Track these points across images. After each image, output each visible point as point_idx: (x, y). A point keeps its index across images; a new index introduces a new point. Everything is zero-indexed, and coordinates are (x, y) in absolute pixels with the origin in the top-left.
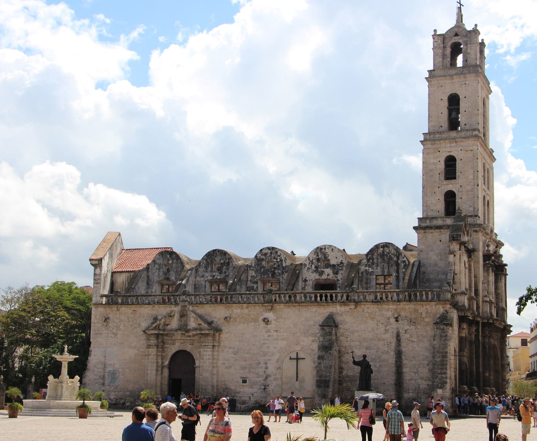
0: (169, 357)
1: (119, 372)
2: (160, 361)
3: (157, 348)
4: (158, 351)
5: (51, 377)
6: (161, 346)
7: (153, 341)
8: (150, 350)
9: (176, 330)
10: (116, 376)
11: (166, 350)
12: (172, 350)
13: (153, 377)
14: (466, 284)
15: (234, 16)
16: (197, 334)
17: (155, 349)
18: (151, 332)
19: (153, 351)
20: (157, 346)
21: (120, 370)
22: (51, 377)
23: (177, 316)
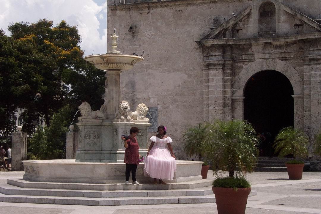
0: (243, 83)
2: (229, 90)
3: (224, 70)
4: (224, 74)
5: (84, 108)
6: (230, 68)
7: (216, 57)
8: (211, 72)
9: (256, 38)
11: (237, 71)
12: (248, 71)
13: (219, 117)
14: (239, 60)
15: (208, 170)
16: (294, 43)
17: (221, 71)
18: (210, 43)
19: (216, 77)
20: (224, 66)
21: (159, 107)
22: (84, 108)
23: (255, 15)
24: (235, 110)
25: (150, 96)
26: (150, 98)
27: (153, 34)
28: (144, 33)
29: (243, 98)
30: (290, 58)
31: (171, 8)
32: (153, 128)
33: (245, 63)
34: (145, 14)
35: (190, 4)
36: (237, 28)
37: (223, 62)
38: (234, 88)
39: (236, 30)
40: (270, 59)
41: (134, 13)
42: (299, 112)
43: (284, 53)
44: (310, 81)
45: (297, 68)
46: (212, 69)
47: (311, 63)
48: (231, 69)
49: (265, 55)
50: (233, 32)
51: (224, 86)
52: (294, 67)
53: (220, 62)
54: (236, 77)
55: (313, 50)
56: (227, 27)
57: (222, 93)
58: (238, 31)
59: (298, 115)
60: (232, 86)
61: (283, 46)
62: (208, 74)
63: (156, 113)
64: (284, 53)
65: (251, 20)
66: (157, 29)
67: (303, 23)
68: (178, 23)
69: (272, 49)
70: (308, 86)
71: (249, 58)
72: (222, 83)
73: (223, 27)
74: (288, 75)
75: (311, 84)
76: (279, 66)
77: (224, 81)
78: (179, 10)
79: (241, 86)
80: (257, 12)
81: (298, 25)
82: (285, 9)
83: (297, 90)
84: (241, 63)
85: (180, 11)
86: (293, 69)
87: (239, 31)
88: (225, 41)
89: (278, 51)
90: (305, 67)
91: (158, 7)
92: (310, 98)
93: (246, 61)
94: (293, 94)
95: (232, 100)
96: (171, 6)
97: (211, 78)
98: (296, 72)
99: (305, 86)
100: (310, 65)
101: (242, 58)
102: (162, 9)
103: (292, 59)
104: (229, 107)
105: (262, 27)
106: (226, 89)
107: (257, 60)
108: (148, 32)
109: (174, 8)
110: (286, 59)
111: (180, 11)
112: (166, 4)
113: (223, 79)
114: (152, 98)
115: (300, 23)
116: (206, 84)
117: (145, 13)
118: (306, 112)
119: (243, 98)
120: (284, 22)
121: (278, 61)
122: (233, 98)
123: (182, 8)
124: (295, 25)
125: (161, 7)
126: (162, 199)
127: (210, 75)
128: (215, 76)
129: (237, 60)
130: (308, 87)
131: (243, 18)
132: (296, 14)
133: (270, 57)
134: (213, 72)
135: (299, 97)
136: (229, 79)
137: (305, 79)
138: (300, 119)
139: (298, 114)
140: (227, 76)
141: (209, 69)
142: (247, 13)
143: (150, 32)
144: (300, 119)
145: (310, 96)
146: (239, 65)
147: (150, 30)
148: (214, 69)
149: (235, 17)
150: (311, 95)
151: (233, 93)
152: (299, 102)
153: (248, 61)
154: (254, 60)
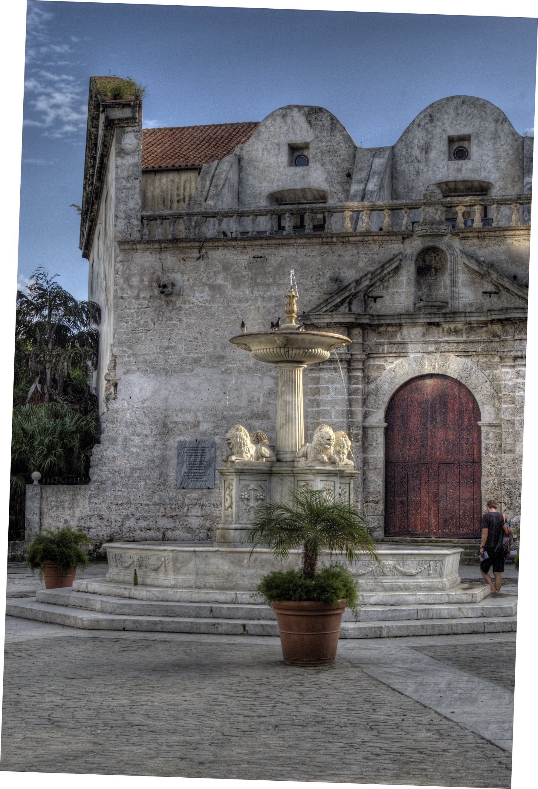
1: (213, 445)
2: (358, 409)
8: (326, 375)
10: (207, 458)
17: (342, 373)
21: (217, 439)
24: (368, 448)
25: (201, 419)
26: (199, 422)
27: (206, 300)
28: (189, 296)
29: (385, 425)
30: (474, 353)
31: (244, 251)
32: (204, 479)
33: (390, 360)
34: (192, 260)
35: (283, 245)
36: (375, 294)
37: (349, 356)
38: (367, 407)
39: (372, 297)
40: (436, 354)
41: (170, 259)
42: (491, 455)
43: (465, 342)
44: (514, 397)
45: (488, 371)
46: (326, 369)
47: (517, 363)
48: (363, 370)
49: (427, 345)
50: (365, 301)
51: (350, 403)
52: (483, 370)
53: (343, 356)
54: (372, 386)
55: (521, 340)
56: (357, 290)
57: (345, 416)
58: (375, 299)
59: (489, 460)
60: (364, 402)
61: (462, 330)
62: (319, 378)
63: (212, 452)
64: (465, 342)
65: (401, 279)
66: (215, 288)
67: (500, 291)
68: (259, 280)
69: (441, 335)
70: (510, 406)
71: (397, 351)
72: (346, 397)
73: (350, 290)
74: (470, 384)
75: (516, 402)
76: (454, 366)
77: (350, 393)
78: (260, 255)
79: (381, 402)
80: (413, 265)
81: (490, 293)
82: (467, 263)
83: (487, 415)
84: (382, 359)
85: (261, 257)
86: (480, 374)
87: (379, 300)
88: (353, 316)
89: (452, 338)
90: (503, 370)
91: (218, 247)
92: (513, 427)
93: (391, 355)
94: (480, 421)
95: (364, 428)
96: (245, 247)
97: (325, 386)
98: (486, 379)
99: (504, 406)
100: (514, 367)
101: (383, 350)
102: (226, 251)
103: (478, 355)
104: (358, 442)
105: (420, 293)
106: (353, 409)
107: (412, 356)
108: (197, 294)
109: (251, 252)
110: (466, 354)
111: (261, 257)
112: (234, 243)
113: (349, 389)
114: (204, 421)
115: (494, 290)
116: (312, 398)
117: (192, 258)
118: (506, 455)
119: (385, 425)
120: (463, 286)
121: (452, 357)
122: (367, 424)
123: (266, 251)
124: (484, 293)
125: (223, 249)
126: (457, 624)
127: (322, 381)
128: (332, 382)
129: (85, 640)
130: (509, 408)
131: (385, 276)
132: (489, 273)
133: (436, 349)
134: (329, 374)
135: (491, 426)
136: (358, 389)
137: (503, 393)
138: (493, 466)
139: (489, 457)
140: (355, 384)
141: (321, 369)
142: (394, 266)
143: (202, 295)
144: (493, 466)
145: (513, 424)
146: (378, 363)
147: (203, 292)
148: (330, 368)
149: (373, 273)
150: (516, 422)
151: (366, 415)
152: (491, 434)
153: (393, 355)
154: (405, 354)
